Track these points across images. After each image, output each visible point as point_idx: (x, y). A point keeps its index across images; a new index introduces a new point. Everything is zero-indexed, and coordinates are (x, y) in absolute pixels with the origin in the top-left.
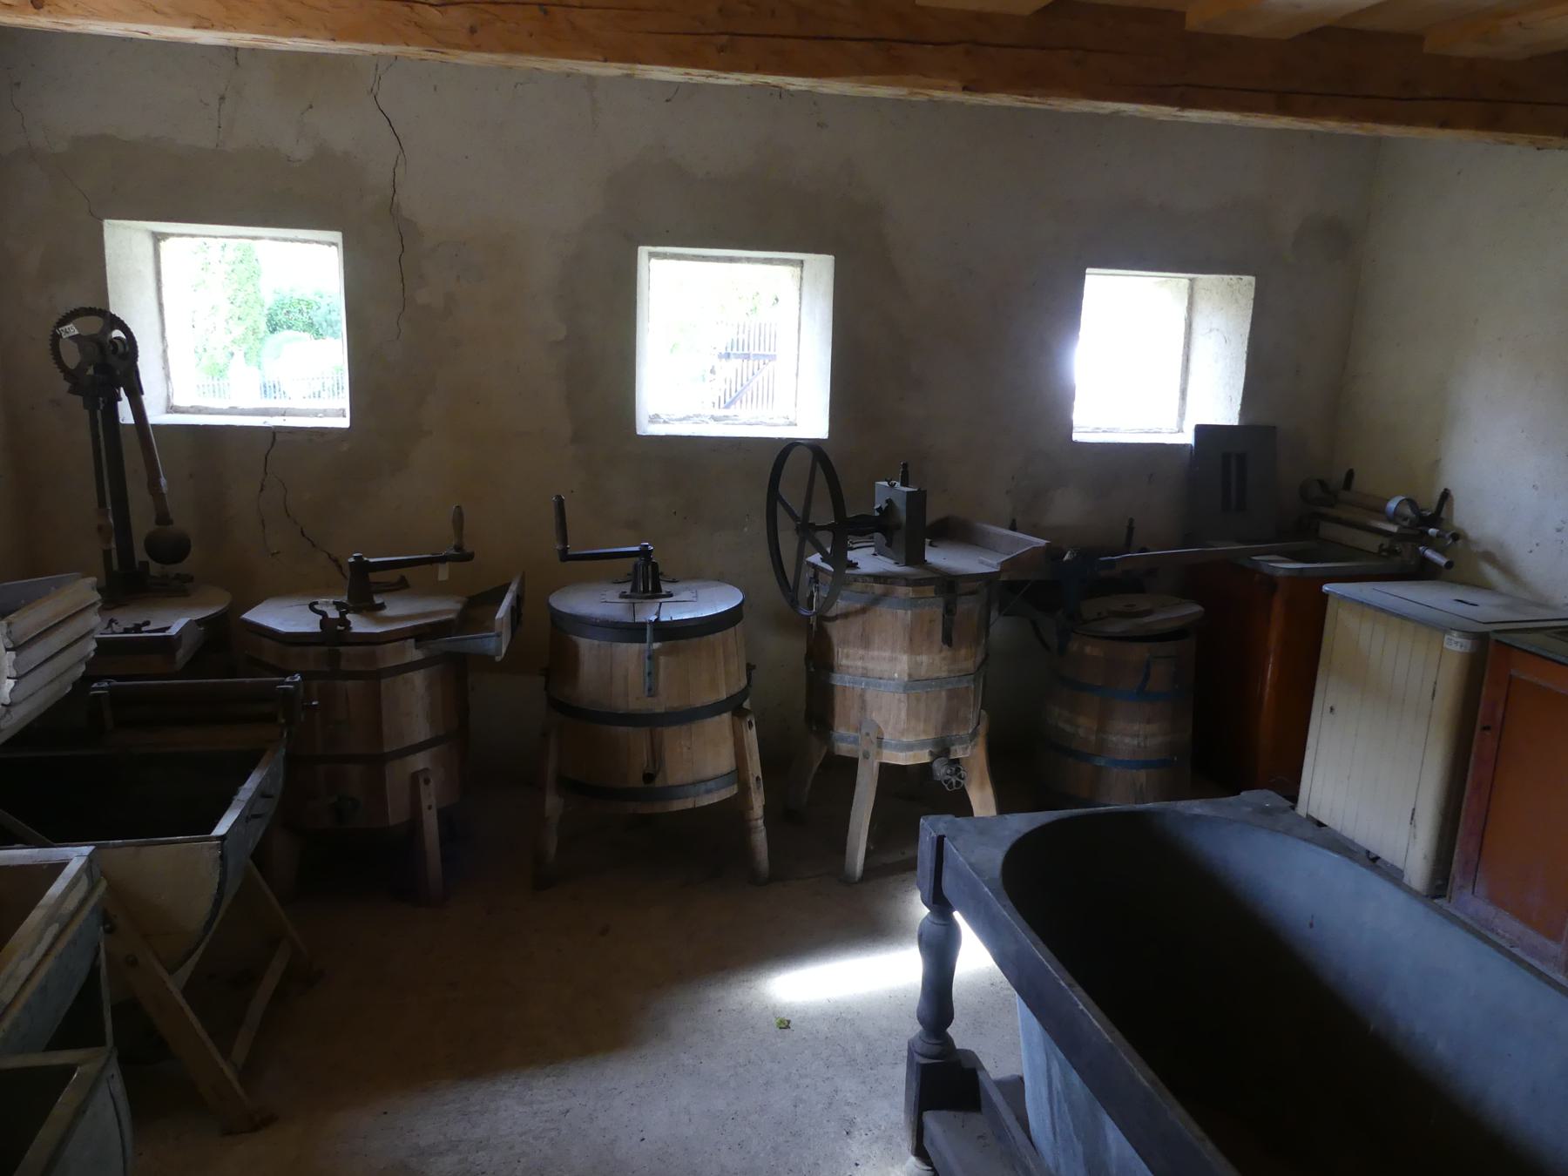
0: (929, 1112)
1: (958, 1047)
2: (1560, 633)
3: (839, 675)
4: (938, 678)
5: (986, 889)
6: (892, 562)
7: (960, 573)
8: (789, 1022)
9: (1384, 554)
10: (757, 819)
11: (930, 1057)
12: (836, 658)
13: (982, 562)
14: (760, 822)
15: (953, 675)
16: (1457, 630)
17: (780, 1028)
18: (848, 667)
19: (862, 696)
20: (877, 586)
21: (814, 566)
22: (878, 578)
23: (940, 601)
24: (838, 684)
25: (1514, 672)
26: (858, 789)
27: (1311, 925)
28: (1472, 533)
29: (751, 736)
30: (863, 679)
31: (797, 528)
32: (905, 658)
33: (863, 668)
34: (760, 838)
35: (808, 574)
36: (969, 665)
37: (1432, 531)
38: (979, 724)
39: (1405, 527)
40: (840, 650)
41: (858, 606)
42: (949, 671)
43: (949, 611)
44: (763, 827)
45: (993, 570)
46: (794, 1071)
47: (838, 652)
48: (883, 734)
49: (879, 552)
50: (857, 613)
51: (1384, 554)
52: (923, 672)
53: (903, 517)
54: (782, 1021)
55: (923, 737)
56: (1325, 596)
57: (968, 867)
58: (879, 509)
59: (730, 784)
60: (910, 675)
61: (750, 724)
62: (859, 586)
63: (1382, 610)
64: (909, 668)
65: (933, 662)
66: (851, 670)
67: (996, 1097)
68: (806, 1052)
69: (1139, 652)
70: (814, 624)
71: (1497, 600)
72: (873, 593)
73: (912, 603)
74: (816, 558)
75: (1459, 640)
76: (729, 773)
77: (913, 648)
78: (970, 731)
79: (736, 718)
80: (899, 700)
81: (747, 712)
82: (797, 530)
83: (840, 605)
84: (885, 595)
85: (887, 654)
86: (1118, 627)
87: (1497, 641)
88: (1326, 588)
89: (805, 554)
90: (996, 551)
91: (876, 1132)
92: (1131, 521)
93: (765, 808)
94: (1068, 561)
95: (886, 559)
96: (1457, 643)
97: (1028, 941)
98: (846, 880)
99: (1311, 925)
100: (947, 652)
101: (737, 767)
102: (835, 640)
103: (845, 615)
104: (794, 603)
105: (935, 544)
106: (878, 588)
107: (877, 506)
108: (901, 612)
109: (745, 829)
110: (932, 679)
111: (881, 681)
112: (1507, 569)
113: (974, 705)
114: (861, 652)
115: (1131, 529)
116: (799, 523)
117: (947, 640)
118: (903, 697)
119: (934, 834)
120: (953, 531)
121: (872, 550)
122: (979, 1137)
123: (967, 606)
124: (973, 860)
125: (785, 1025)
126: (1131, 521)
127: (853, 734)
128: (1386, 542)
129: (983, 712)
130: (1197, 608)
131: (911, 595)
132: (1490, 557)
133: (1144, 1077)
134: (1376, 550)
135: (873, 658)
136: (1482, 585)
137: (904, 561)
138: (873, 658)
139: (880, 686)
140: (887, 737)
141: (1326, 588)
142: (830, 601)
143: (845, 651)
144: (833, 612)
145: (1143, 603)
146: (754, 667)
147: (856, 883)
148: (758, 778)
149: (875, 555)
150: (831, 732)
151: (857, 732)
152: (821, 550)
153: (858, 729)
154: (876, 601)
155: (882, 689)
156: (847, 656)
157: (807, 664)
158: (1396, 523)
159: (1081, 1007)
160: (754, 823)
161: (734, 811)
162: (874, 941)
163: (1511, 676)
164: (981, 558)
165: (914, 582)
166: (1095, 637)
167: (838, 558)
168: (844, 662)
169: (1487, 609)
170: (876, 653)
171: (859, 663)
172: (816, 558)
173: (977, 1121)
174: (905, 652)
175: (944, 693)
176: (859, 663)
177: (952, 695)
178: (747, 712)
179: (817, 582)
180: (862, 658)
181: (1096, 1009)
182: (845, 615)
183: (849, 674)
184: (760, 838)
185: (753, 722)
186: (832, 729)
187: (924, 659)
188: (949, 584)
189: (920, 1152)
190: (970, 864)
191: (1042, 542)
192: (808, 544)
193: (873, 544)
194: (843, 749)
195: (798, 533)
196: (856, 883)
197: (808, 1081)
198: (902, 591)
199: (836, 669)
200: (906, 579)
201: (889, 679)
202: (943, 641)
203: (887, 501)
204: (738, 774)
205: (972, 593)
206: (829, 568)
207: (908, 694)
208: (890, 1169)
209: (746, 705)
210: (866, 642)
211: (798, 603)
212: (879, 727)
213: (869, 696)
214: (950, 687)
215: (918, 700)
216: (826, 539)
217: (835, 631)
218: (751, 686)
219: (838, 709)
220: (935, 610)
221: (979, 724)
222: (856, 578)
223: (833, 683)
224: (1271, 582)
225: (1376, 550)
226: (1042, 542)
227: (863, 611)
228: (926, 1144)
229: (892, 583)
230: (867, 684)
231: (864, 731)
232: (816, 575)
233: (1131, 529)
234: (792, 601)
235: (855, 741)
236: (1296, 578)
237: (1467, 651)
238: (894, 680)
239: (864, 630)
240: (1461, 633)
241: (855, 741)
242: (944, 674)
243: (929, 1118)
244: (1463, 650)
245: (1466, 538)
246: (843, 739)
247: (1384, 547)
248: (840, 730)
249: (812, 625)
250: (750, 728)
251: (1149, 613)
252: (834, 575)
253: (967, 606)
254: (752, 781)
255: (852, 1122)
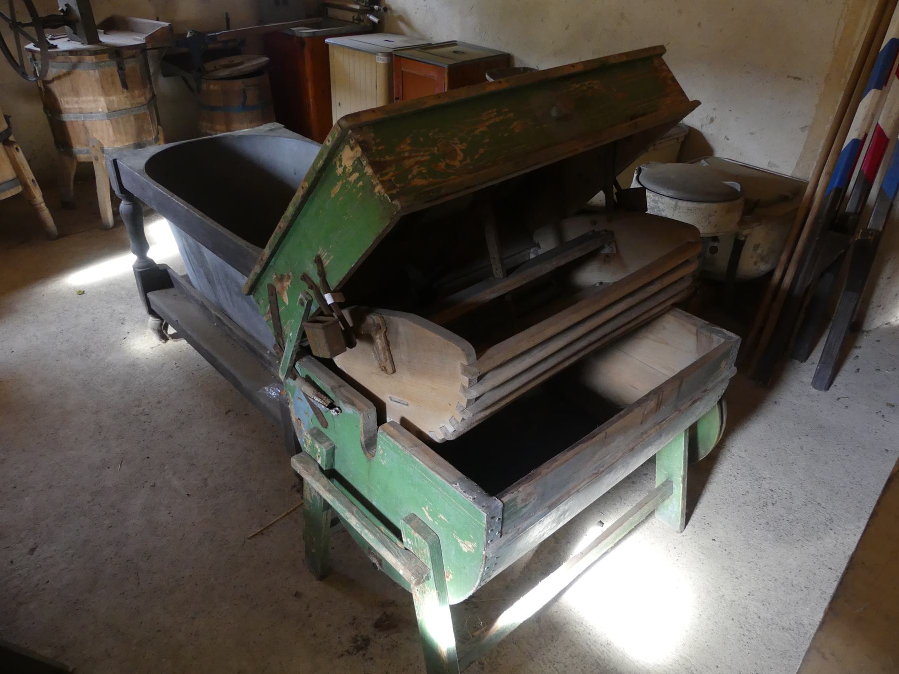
0: (150, 293)
1: (157, 264)
2: (422, 49)
3: (65, 115)
4: (125, 109)
5: (136, 173)
6: (80, 43)
7: (121, 46)
8: (84, 291)
9: (356, 21)
10: (40, 204)
11: (143, 268)
12: (61, 104)
13: (135, 39)
14: (43, 205)
15: (134, 106)
16: (380, 52)
17: (80, 294)
18: (70, 109)
19: (83, 125)
20: (72, 57)
21: (30, 50)
22: (71, 52)
23: (114, 63)
24: (67, 120)
25: (403, 69)
26: (97, 179)
27: (295, 174)
28: (393, 7)
29: (20, 157)
30: (81, 115)
31: (11, 26)
32: (102, 99)
33: (79, 108)
34: (46, 214)
35: (30, 56)
36: (142, 100)
37: (376, 7)
38: (158, 133)
39: (364, 6)
40: (62, 100)
41: (64, 71)
42: (132, 104)
43: (121, 68)
44: (46, 208)
45: (142, 43)
46: (90, 309)
47: (61, 101)
48: (103, 145)
49: (71, 39)
50: (65, 75)
51: (356, 21)
52: (116, 106)
53: (78, 13)
54: (80, 292)
55: (127, 144)
56: (327, 45)
57: (128, 168)
58: (62, 11)
59: (16, 185)
60: (108, 109)
61: (17, 149)
62: (60, 58)
63: (357, 50)
64: (107, 105)
65: (120, 99)
66: (72, 111)
67: (183, 282)
68: (96, 300)
69: (238, 84)
70: (42, 87)
71: (405, 38)
72: (71, 62)
73: (97, 65)
74: (31, 46)
75: (381, 57)
76: (12, 180)
77: (106, 93)
78: (154, 137)
79: (6, 147)
80: (106, 124)
81: (12, 143)
82: (11, 27)
83: (52, 72)
84: (80, 62)
85: (91, 98)
86: (224, 73)
87: (395, 55)
88: (327, 40)
89: (22, 45)
90: (137, 32)
91: (136, 320)
92: (227, 14)
93: (44, 197)
94: (190, 37)
95: (75, 42)
96: (381, 59)
97: (155, 186)
98: (106, 228)
99: (295, 174)
100: (126, 93)
101: (17, 175)
102: (57, 94)
103: (59, 78)
104: (24, 75)
105: (107, 33)
106: (74, 58)
107: (60, 9)
108: (92, 72)
109: (34, 211)
110: (123, 110)
111: (92, 114)
112: (408, 24)
113: (152, 122)
114: (75, 99)
115: (228, 20)
116: (11, 22)
117: (125, 86)
118: (108, 122)
119: (111, 159)
120: (113, 25)
121: (67, 39)
122: (174, 295)
123: (130, 65)
124: (130, 165)
125: (81, 293)
126: (227, 14)
127: (85, 148)
128: (356, 15)
129: (160, 128)
130: (266, 59)
131: (94, 60)
132: (401, 18)
133: (199, 215)
134: (351, 20)
135: (83, 102)
136: (398, 32)
137: (87, 42)
138: (83, 102)
139: (93, 117)
140: (105, 147)
141: (327, 40)
142: (44, 72)
143: (65, 99)
144: (49, 77)
145: (237, 59)
146: (10, 117)
147: (111, 229)
148: (33, 180)
149: (69, 41)
150: (72, 149)
151: (87, 146)
152: (33, 41)
153: (87, 145)
154: (75, 66)
155: (94, 119)
156: (68, 103)
157: (46, 112)
158: (359, 4)
159: (176, 201)
160: (38, 206)
161: (24, 198)
162: (126, 251)
163: (402, 71)
164: (134, 37)
165: (95, 53)
166: (214, 79)
167: (42, 43)
168: (67, 106)
169: (397, 42)
170: (84, 98)
171: (76, 106)
172: (31, 46)
173: (171, 291)
174: (102, 96)
175: (132, 118)
176: (76, 106)
177: (137, 118)
178: (12, 143)
179: (35, 60)
180: (77, 102)
181: (181, 199)
182: (59, 78)
183: (72, 113)
184: (46, 214)
185: (19, 148)
186: (72, 148)
187: (114, 98)
188: (116, 52)
189: (151, 312)
190: (129, 167)
191: (167, 24)
192: (21, 37)
193: (66, 36)
194: (82, 157)
195: (12, 30)
196: (111, 229)
197: (98, 310)
198: (89, 59)
199: (63, 112)
200: (89, 51)
201: (97, 113)
202: (123, 87)
203: (66, 5)
204: (19, 178)
205: (133, 57)
206: (38, 49)
207: (111, 121)
208: (145, 330)
209: (11, 138)
210: (76, 92)
211: (27, 75)
212: (100, 142)
213: (88, 124)
214: (134, 113)
215: (117, 122)
216: (31, 31)
217: (56, 88)
218: (11, 128)
219: (72, 134)
220: (112, 68)
221: (158, 133)
222: (58, 54)
223: (64, 120)
224: (301, 41)
225: (351, 20)
226: (167, 24)
227: (68, 73)
228: (153, 307)
229: (81, 55)
230: (85, 117)
231: (91, 145)
232: (33, 56)
233: (228, 20)
234: (22, 74)
235: (88, 152)
236: (313, 37)
237: (386, 62)
238: (100, 112)
239: (73, 86)
240: (382, 54)
241: (88, 152)
242: (129, 106)
243: (150, 295)
244: (384, 62)
245: (391, 10)
246: (81, 152)
247: (355, 18)
248: (77, 148)
249: (41, 87)
250: (18, 152)
251: (241, 63)
252: (41, 53)
253: (130, 65)
254: (29, 182)
255: (124, 319)
